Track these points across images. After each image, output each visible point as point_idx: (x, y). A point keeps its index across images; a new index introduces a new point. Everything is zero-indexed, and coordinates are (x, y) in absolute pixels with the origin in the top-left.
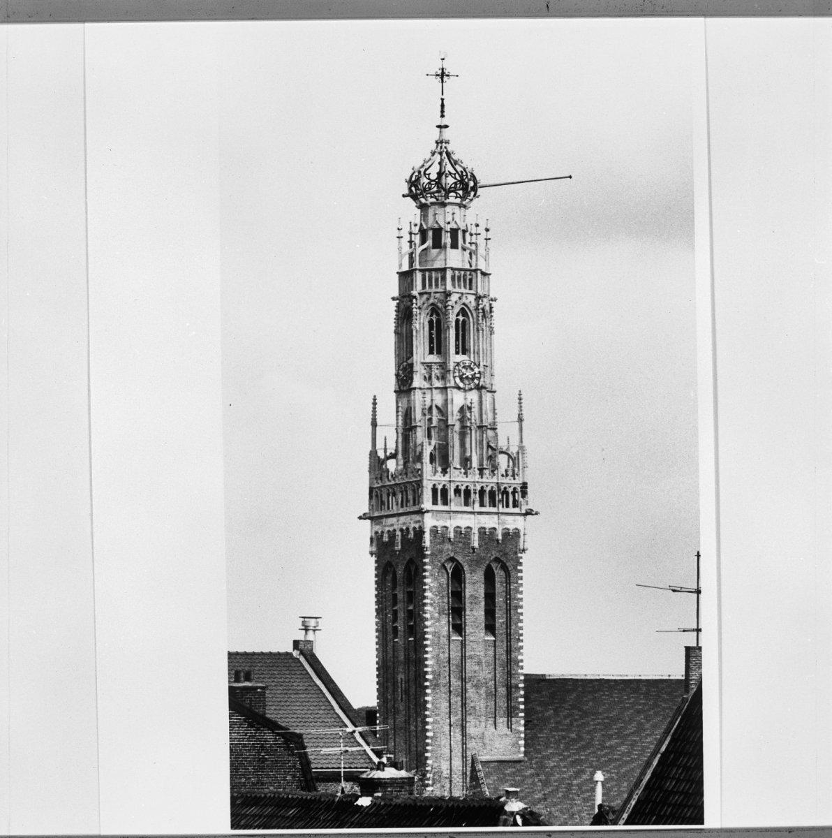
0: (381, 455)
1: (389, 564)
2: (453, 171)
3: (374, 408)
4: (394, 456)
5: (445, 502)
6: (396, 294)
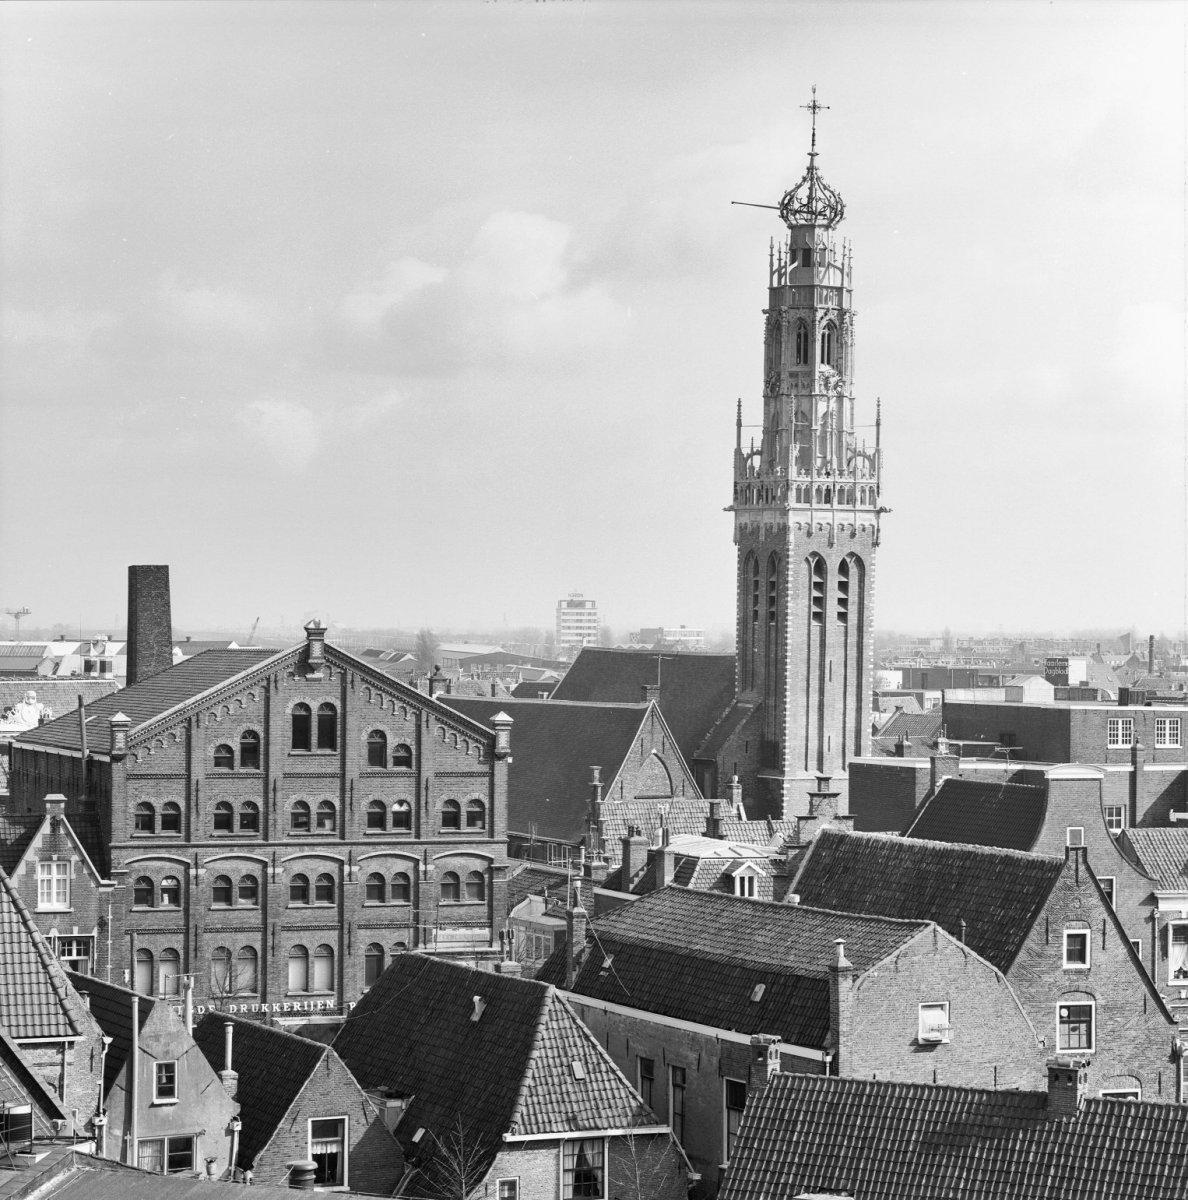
0: (746, 451)
1: (751, 552)
2: (823, 197)
3: (739, 409)
4: (759, 453)
5: (808, 500)
6: (767, 307)
